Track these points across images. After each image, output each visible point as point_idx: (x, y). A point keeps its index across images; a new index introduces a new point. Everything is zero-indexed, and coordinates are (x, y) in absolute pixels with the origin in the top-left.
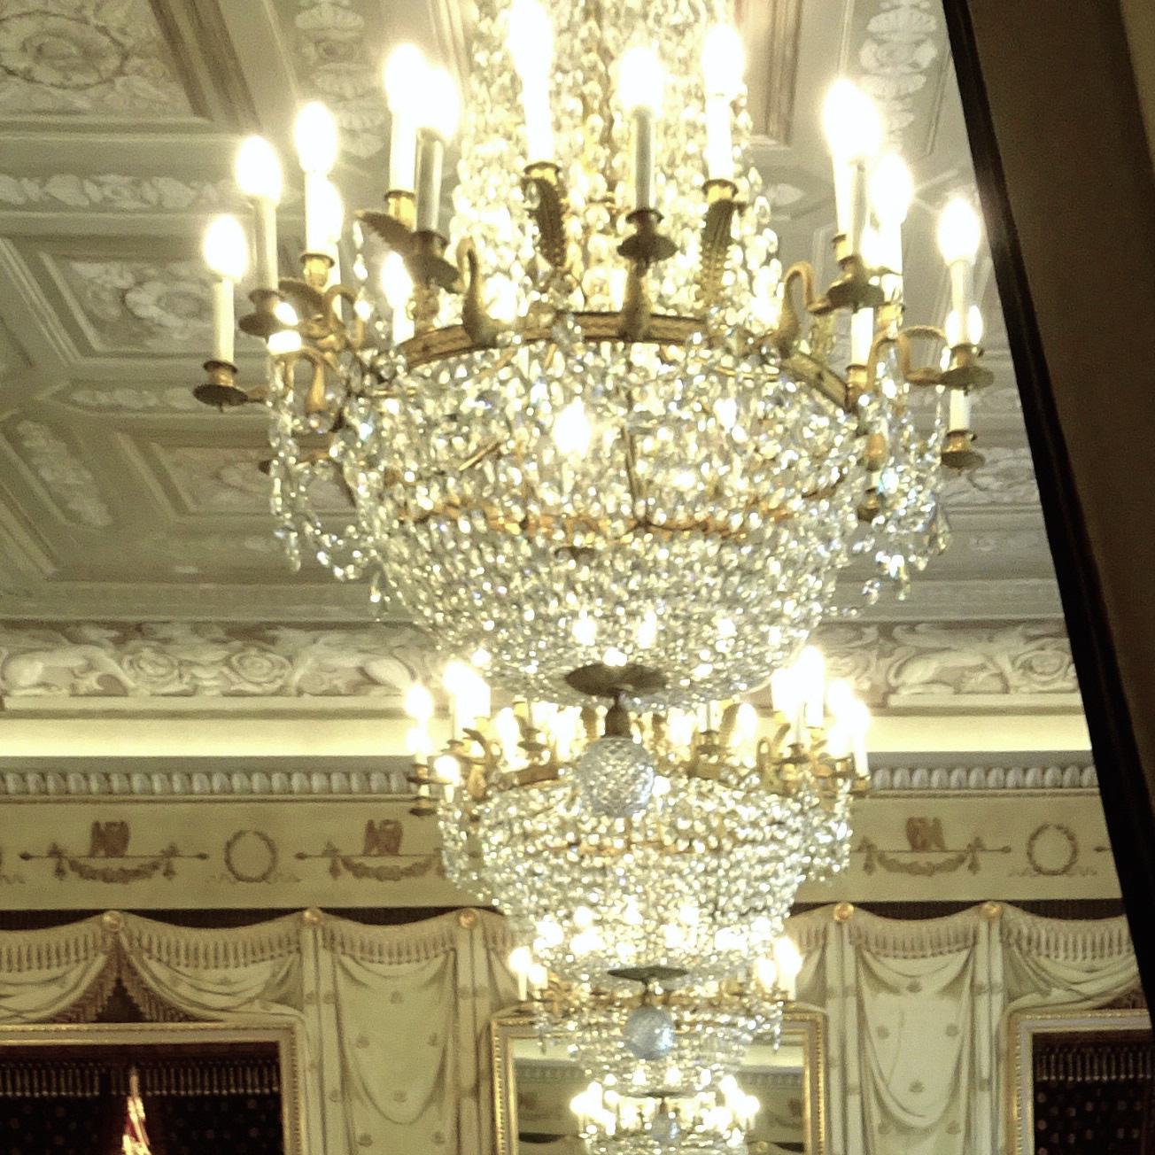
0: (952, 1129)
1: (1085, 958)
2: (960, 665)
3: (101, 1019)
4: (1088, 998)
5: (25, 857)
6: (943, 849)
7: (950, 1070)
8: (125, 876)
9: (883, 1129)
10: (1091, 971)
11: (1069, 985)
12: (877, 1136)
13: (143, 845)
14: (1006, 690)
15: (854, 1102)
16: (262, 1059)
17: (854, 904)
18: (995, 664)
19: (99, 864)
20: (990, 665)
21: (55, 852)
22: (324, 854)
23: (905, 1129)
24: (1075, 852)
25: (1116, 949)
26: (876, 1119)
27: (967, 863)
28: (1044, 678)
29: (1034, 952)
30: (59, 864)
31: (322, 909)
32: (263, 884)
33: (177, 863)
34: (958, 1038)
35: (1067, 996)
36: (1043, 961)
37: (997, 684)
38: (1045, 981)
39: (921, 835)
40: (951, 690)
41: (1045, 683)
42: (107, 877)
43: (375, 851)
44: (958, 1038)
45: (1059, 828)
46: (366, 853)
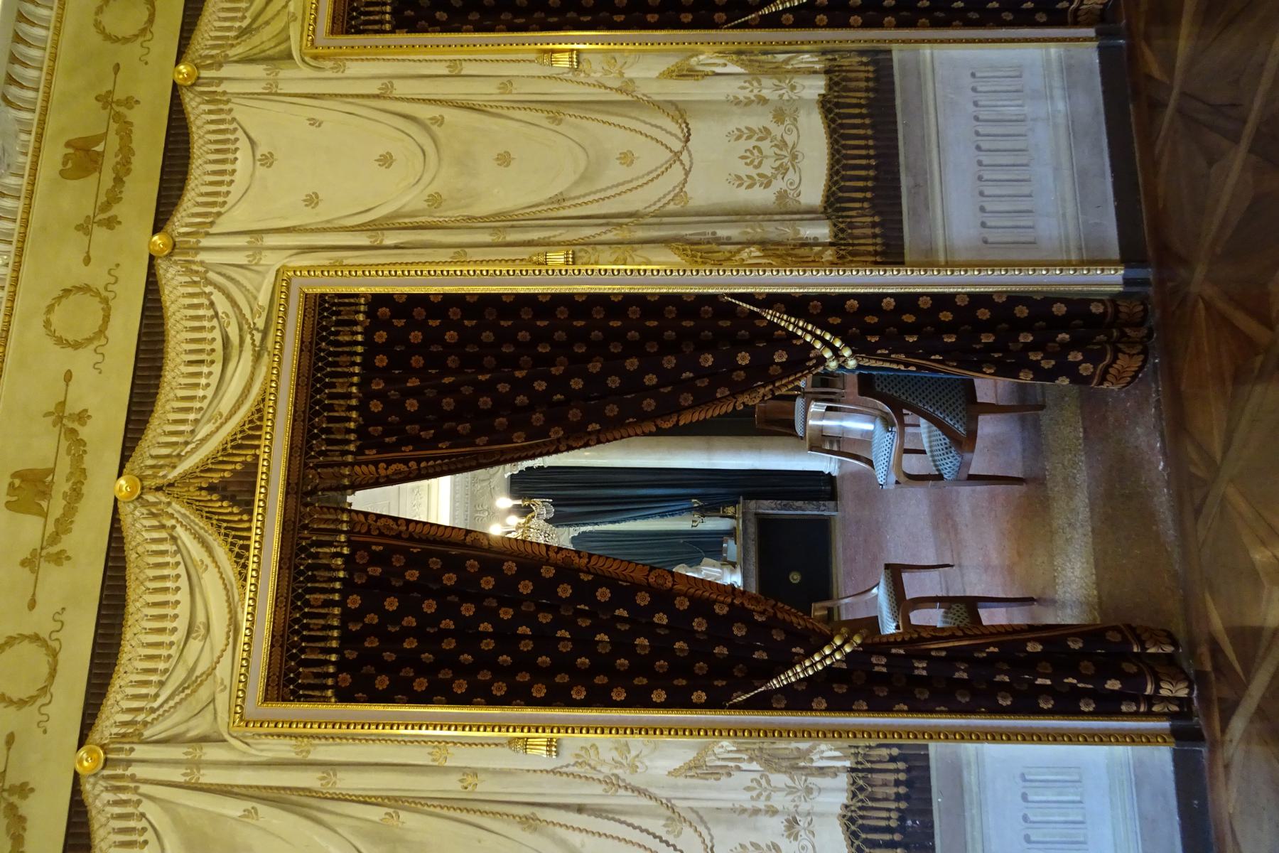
3: (247, 507)
5: (32, 605)
8: (79, 475)
13: (42, 448)
17: (178, 62)
22: (88, 233)
27: (76, 426)
31: (81, 743)
32: (61, 657)
33: (73, 407)
39: (83, 158)
42: (76, 494)
43: (44, 504)
46: (45, 515)
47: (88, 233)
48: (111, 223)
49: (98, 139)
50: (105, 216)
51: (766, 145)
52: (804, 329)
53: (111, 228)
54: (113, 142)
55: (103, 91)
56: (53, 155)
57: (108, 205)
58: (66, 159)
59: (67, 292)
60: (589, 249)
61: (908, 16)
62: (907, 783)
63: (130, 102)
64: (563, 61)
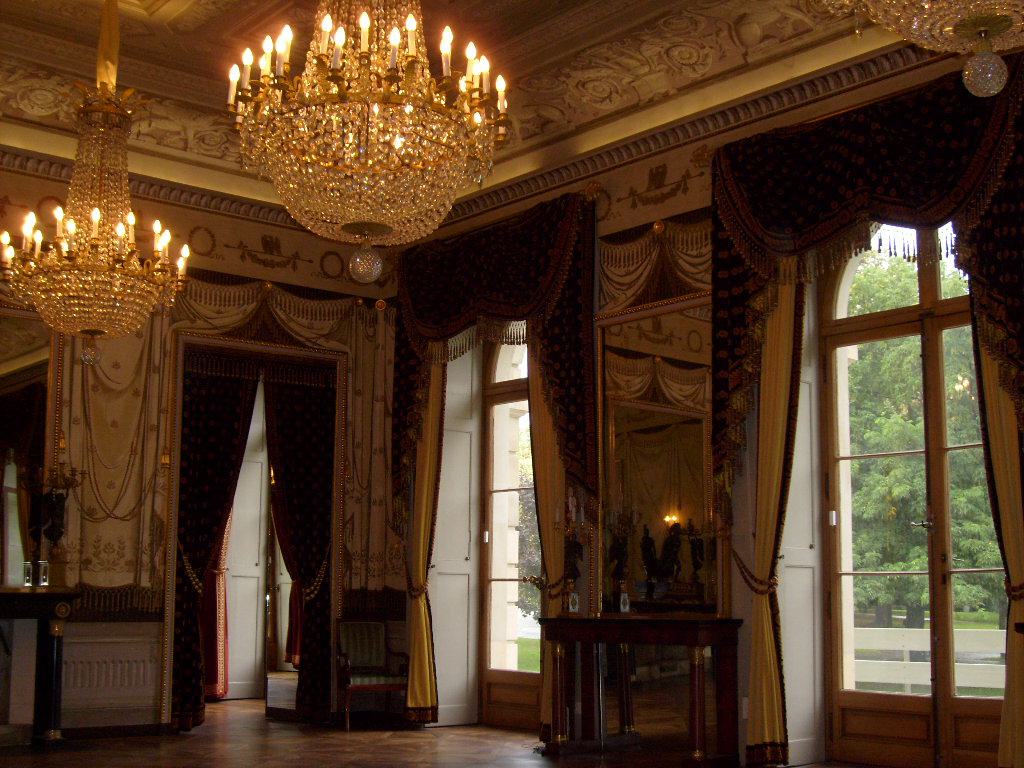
0: (136, 393)
1: (215, 305)
2: (166, 129)
4: (216, 328)
6: (279, 254)
7: (138, 356)
9: (95, 388)
10: (219, 312)
11: (206, 319)
12: (90, 392)
14: (185, 149)
15: (78, 369)
16: (325, 369)
18: (185, 134)
19: (652, 335)
20: (182, 133)
21: (241, 245)
22: (239, 247)
23: (108, 390)
24: (214, 245)
25: (232, 303)
26: (91, 381)
28: (208, 147)
29: (188, 296)
30: (243, 253)
34: (142, 340)
35: (205, 325)
36: (193, 303)
37: (181, 145)
38: (193, 314)
39: (270, 245)
40: (155, 141)
41: (205, 150)
44: (142, 340)
45: (206, 230)
47: (239, 247)
48: (243, 257)
49: (279, 252)
50: (246, 254)
51: (114, 556)
52: (312, 592)
53: (241, 257)
54: (278, 259)
55: (675, 334)
56: (274, 232)
57: (250, 255)
58: (271, 237)
59: (213, 236)
60: (869, 577)
61: (854, 693)
62: (147, 612)
63: (295, 267)
64: (166, 460)
